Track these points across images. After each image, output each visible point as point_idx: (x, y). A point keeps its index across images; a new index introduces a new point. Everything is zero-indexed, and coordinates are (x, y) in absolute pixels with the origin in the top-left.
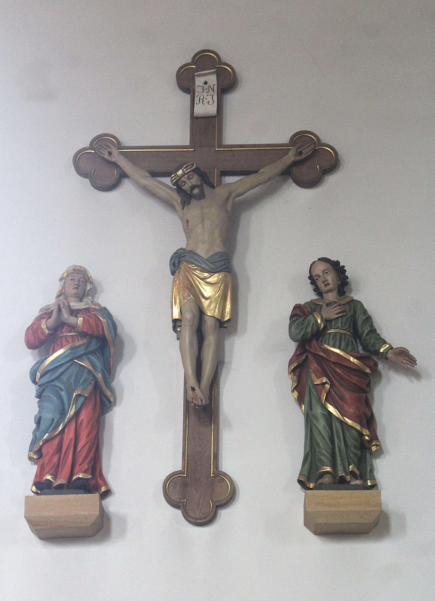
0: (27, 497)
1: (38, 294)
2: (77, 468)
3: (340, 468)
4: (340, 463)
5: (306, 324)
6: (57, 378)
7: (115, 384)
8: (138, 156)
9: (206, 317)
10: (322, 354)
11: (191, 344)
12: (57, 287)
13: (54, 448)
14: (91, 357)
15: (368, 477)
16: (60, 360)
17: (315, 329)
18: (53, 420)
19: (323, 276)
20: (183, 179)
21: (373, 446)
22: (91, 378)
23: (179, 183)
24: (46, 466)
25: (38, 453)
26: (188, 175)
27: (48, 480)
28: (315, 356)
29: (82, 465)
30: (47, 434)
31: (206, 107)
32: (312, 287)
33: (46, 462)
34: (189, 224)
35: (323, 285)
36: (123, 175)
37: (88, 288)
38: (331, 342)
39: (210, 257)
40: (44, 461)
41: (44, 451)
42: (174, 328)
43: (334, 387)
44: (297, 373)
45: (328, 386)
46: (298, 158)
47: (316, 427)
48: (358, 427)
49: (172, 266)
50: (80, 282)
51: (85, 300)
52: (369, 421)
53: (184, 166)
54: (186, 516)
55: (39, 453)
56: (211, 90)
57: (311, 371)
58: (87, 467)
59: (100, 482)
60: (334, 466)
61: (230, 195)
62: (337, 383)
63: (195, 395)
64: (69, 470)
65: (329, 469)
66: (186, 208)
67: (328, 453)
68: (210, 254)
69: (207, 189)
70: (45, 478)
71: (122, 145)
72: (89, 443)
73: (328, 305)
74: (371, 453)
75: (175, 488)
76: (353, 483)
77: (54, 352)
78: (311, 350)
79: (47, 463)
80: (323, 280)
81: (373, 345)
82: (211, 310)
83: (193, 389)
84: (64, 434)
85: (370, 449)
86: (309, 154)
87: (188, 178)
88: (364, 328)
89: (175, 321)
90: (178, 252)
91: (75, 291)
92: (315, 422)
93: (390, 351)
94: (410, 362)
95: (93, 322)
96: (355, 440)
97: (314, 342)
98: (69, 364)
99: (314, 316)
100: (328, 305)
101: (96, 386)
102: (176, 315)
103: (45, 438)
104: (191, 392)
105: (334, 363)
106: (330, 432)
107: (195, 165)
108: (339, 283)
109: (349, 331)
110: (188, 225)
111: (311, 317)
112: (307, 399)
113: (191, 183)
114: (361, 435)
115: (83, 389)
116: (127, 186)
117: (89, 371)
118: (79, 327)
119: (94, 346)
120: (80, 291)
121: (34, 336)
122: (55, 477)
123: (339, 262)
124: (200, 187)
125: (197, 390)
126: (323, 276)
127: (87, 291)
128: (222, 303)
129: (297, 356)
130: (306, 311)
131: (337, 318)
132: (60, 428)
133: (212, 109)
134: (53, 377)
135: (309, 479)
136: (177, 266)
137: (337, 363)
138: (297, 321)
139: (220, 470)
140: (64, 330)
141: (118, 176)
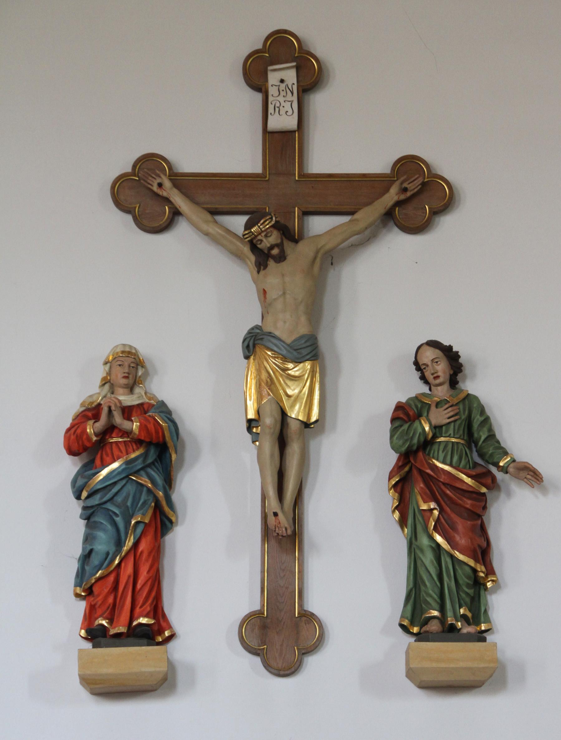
0: (80, 651)
1: (78, 385)
2: (138, 610)
3: (450, 613)
4: (449, 601)
5: (411, 435)
6: (111, 499)
7: (175, 497)
8: (198, 186)
9: (289, 420)
10: (429, 471)
11: (272, 456)
12: (101, 372)
13: (109, 586)
14: (150, 471)
15: (482, 619)
16: (114, 477)
17: (422, 439)
18: (108, 554)
19: (433, 366)
20: (259, 237)
21: (489, 582)
22: (151, 498)
23: (254, 241)
24: (99, 607)
25: (87, 590)
26: (265, 233)
27: (102, 625)
28: (422, 473)
29: (144, 607)
30: (100, 572)
31: (284, 120)
32: (418, 374)
33: (99, 603)
34: (267, 296)
35: (432, 377)
36: (176, 213)
37: (140, 373)
38: (441, 456)
39: (295, 341)
40: (96, 601)
41: (96, 589)
42: (249, 429)
43: (443, 514)
44: (399, 489)
45: (436, 513)
46: (402, 197)
47: (422, 561)
48: (472, 563)
49: (246, 351)
50: (130, 367)
51: (137, 390)
52: (483, 553)
53: (262, 221)
54: (267, 666)
55: (90, 591)
56: (289, 93)
57: (416, 491)
58: (148, 609)
59: (164, 624)
60: (442, 609)
61: (317, 252)
62: (448, 510)
63: (278, 521)
64: (129, 614)
65: (435, 613)
66: (262, 272)
67: (435, 593)
68: (293, 338)
69: (288, 246)
70: (96, 623)
71: (175, 171)
72: (151, 580)
73: (438, 405)
74: (486, 589)
75: (252, 631)
76: (465, 631)
77: (104, 465)
78: (416, 465)
79: (101, 605)
80: (433, 372)
81: (492, 455)
82: (296, 413)
83: (276, 514)
84: (121, 568)
85: (485, 585)
86: (416, 190)
87: (266, 236)
88: (481, 433)
89: (250, 421)
90: (253, 331)
91: (124, 381)
92: (421, 555)
93: (512, 465)
94: (535, 478)
95: (151, 427)
96: (468, 577)
97: (420, 454)
98: (124, 482)
99: (421, 423)
100: (438, 405)
101: (158, 507)
102: (251, 415)
103: (98, 575)
104: (274, 518)
105: (444, 484)
106: (438, 568)
107: (274, 218)
108: (452, 372)
109: (463, 439)
110: (265, 297)
111: (417, 423)
112: (410, 521)
113: (269, 242)
114: (475, 571)
115: (144, 514)
116: (182, 228)
117: (149, 491)
118: (135, 434)
119: (152, 455)
120: (131, 381)
121: (78, 443)
122: (111, 621)
123: (452, 347)
124: (280, 246)
125: (281, 515)
126: (433, 366)
127: (138, 377)
128: (308, 403)
129: (398, 468)
130: (411, 413)
131: (449, 423)
132: (117, 562)
133: (291, 123)
134: (105, 499)
135: (412, 623)
136: (252, 351)
137: (448, 484)
138: (400, 430)
139: (305, 609)
140: (114, 435)
141: (171, 216)
